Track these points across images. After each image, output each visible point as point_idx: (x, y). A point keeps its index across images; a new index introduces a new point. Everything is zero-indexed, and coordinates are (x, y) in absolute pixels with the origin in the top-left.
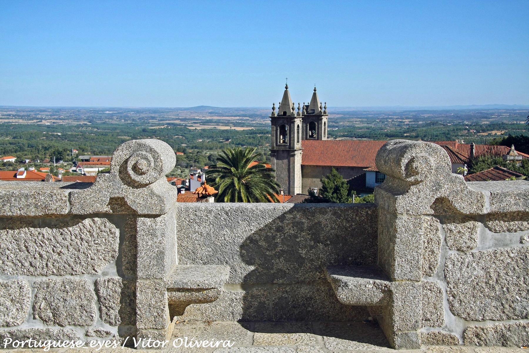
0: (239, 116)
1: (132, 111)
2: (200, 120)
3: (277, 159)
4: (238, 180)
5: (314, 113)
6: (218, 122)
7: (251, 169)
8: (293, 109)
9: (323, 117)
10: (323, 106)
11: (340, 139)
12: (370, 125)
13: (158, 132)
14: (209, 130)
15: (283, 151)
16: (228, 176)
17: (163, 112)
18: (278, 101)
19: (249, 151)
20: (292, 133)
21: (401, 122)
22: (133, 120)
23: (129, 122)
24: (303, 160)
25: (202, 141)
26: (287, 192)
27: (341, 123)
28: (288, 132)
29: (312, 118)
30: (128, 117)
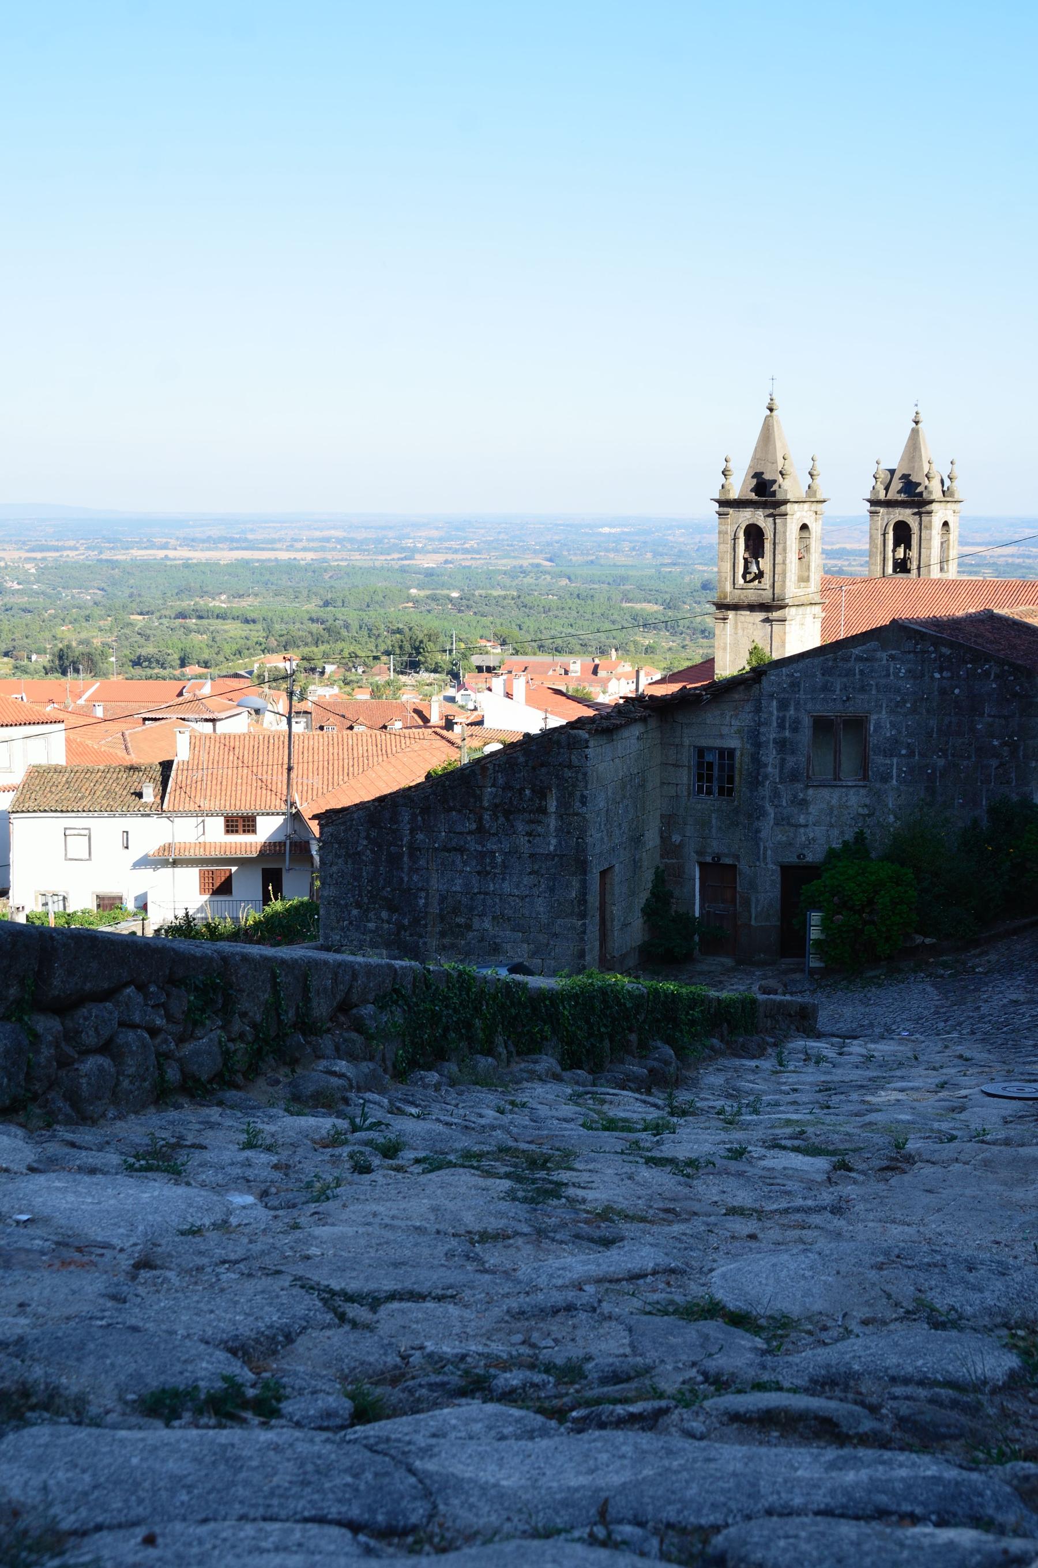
1: (679, 528)
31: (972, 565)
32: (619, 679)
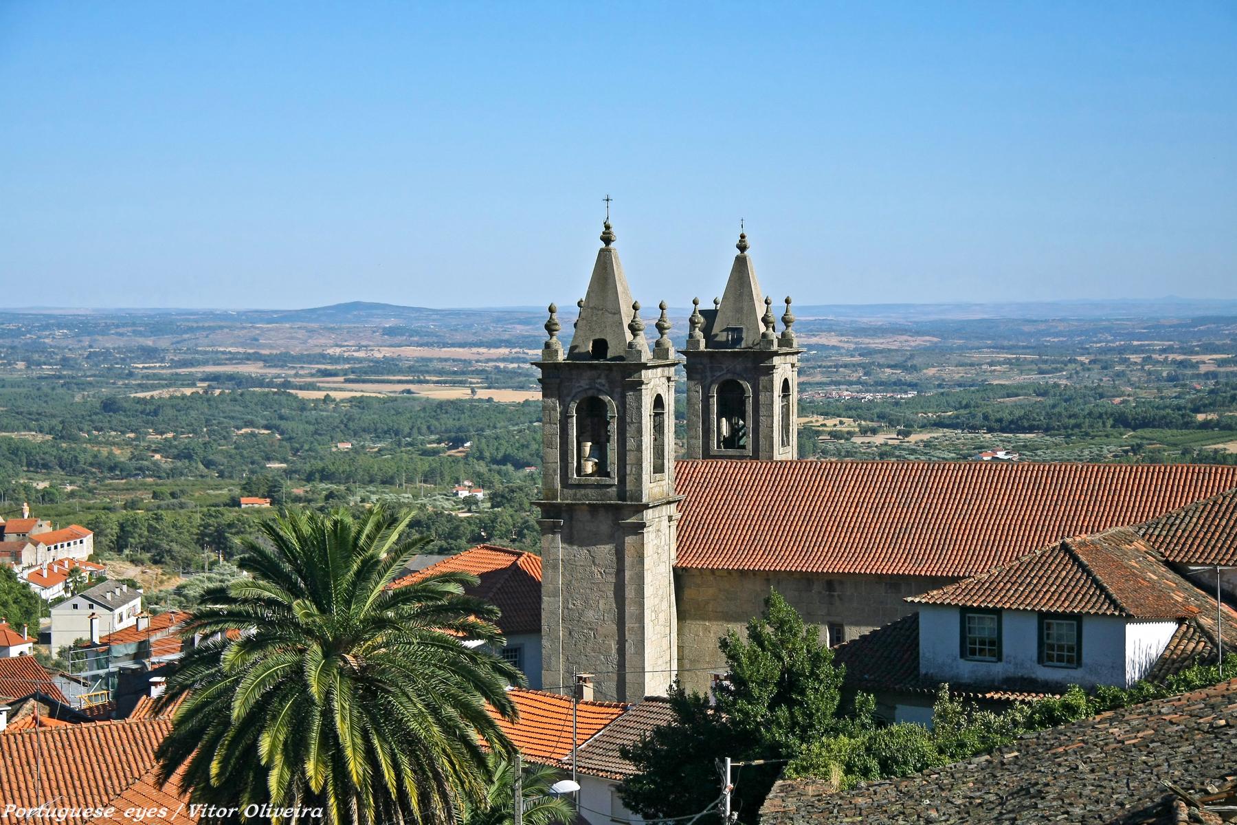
0: (508, 344)
1: (59, 326)
2: (347, 360)
3: (569, 540)
4: (326, 655)
5: (740, 340)
6: (419, 371)
7: (383, 604)
8: (634, 329)
9: (776, 361)
10: (776, 316)
11: (925, 436)
12: (1051, 379)
13: (170, 412)
14: (384, 401)
15: (593, 509)
16: (282, 639)
17: (190, 330)
18: (571, 292)
19: (378, 527)
20: (631, 431)
21: (1181, 364)
22: (65, 362)
23: (47, 370)
24: (682, 546)
25: (355, 450)
26: (611, 687)
27: (931, 372)
28: (613, 427)
29: (730, 365)
30: (42, 349)
31: (455, 373)
32: (36, 544)
